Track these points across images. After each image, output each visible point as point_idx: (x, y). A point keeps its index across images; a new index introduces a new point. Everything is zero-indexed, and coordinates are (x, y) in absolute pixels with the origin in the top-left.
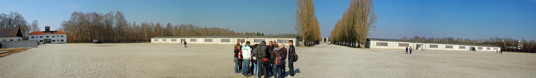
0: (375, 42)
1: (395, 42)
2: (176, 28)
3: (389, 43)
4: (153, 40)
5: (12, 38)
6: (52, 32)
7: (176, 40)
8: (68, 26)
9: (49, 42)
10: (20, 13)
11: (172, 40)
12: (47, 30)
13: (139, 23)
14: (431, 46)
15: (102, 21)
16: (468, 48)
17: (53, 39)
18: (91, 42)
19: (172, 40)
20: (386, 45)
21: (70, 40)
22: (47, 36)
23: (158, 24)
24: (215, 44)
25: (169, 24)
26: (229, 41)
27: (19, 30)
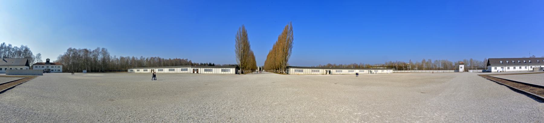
0: (294, 69)
1: (309, 70)
2: (147, 59)
3: (304, 70)
4: (129, 70)
5: (21, 67)
6: (52, 64)
7: (147, 70)
8: (65, 58)
9: (48, 71)
10: (28, 47)
11: (144, 71)
12: (48, 61)
13: (118, 57)
14: (205, 71)
15: (91, 56)
16: (190, 70)
17: (52, 69)
18: (81, 71)
19: (144, 71)
20: (302, 71)
21: (65, 70)
22: (47, 67)
23: (133, 58)
24: (215, 74)
25: (471, 59)
26: (187, 70)
27: (27, 62)
